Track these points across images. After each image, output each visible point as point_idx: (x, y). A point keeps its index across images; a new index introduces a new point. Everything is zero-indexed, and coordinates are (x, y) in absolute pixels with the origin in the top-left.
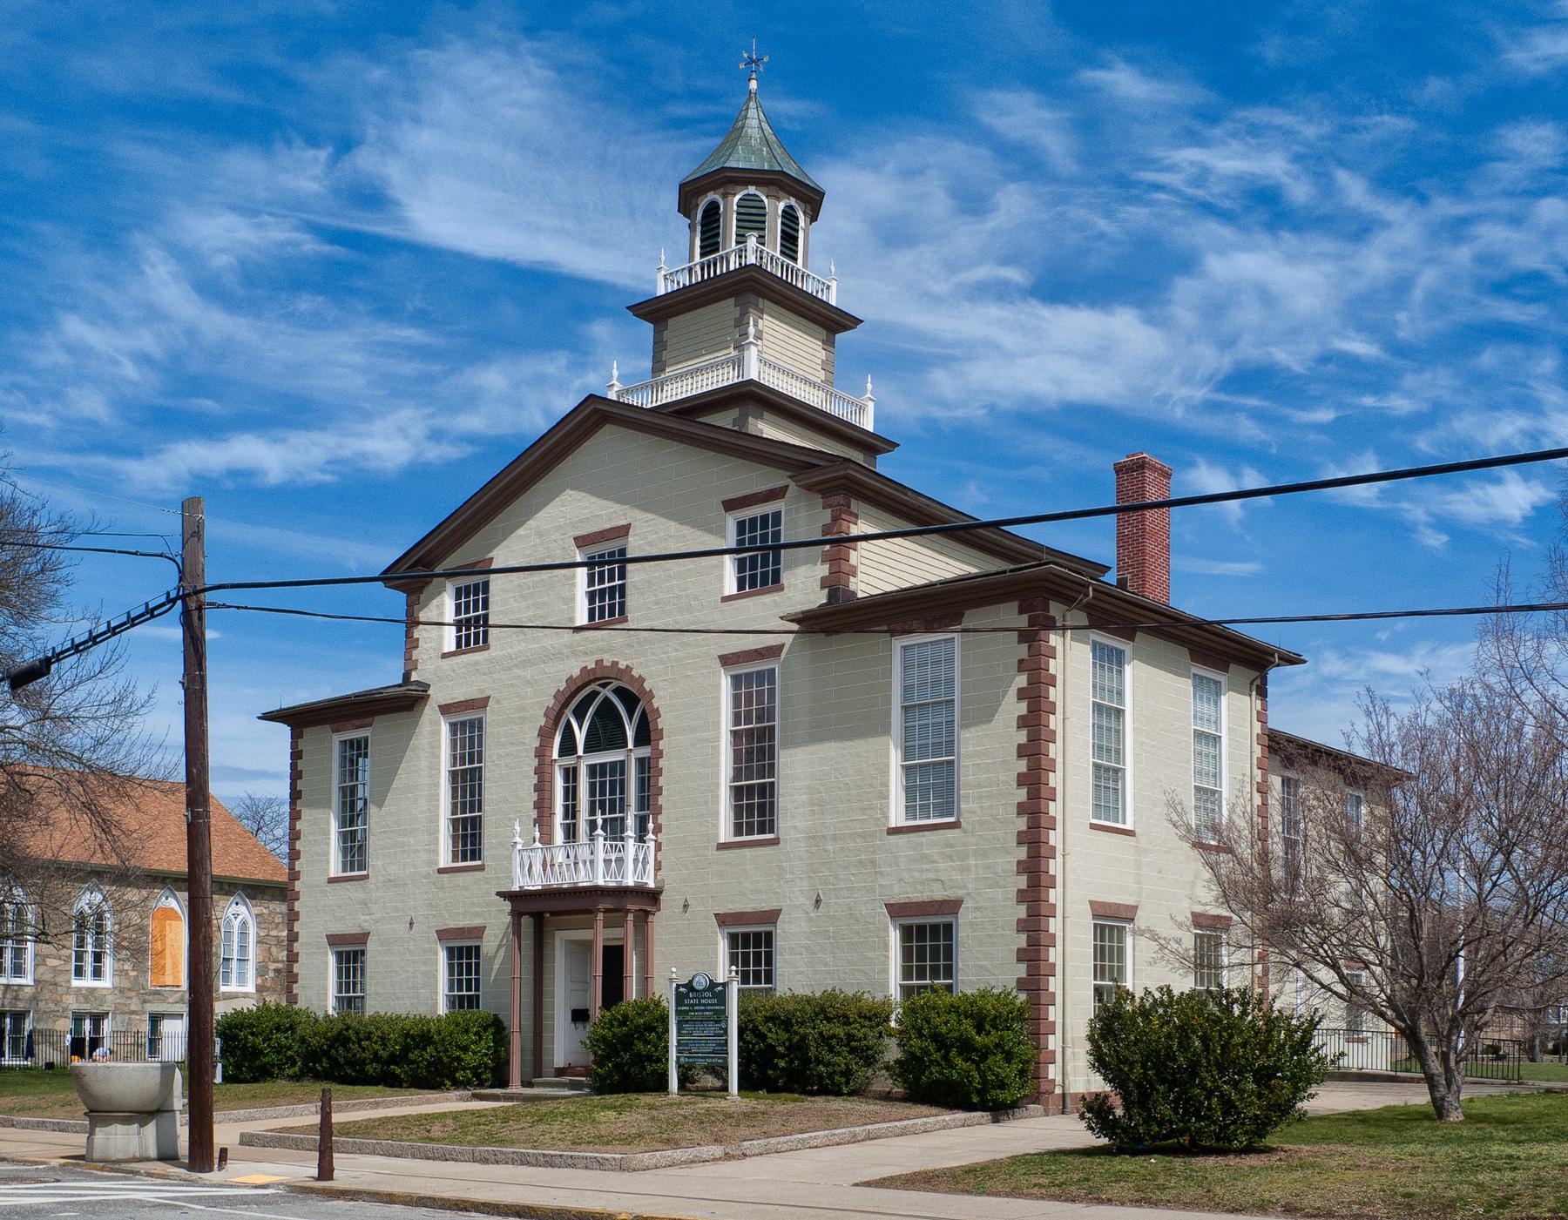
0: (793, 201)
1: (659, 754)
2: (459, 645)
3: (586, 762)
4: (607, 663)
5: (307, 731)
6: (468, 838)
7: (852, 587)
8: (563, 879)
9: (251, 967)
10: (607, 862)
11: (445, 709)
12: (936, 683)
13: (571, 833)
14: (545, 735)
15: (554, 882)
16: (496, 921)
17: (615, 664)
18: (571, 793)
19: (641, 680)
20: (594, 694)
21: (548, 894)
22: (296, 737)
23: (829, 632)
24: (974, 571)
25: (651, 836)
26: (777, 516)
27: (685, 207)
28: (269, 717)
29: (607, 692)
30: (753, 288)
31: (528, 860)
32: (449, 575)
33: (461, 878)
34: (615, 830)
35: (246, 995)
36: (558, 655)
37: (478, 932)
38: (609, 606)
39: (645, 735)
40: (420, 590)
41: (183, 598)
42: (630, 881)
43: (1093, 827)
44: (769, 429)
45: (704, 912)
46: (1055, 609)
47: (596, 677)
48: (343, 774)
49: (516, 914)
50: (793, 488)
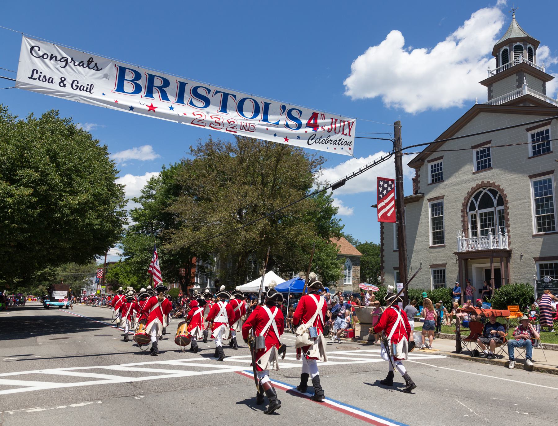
0: (530, 45)
3: (479, 212)
4: (485, 182)
6: (439, 237)
9: (351, 278)
10: (493, 242)
11: (429, 200)
13: (475, 234)
15: (470, 249)
17: (489, 182)
19: (499, 186)
20: (481, 192)
21: (468, 253)
25: (506, 234)
26: (547, 131)
32: (429, 162)
35: (350, 285)
36: (467, 181)
40: (420, 167)
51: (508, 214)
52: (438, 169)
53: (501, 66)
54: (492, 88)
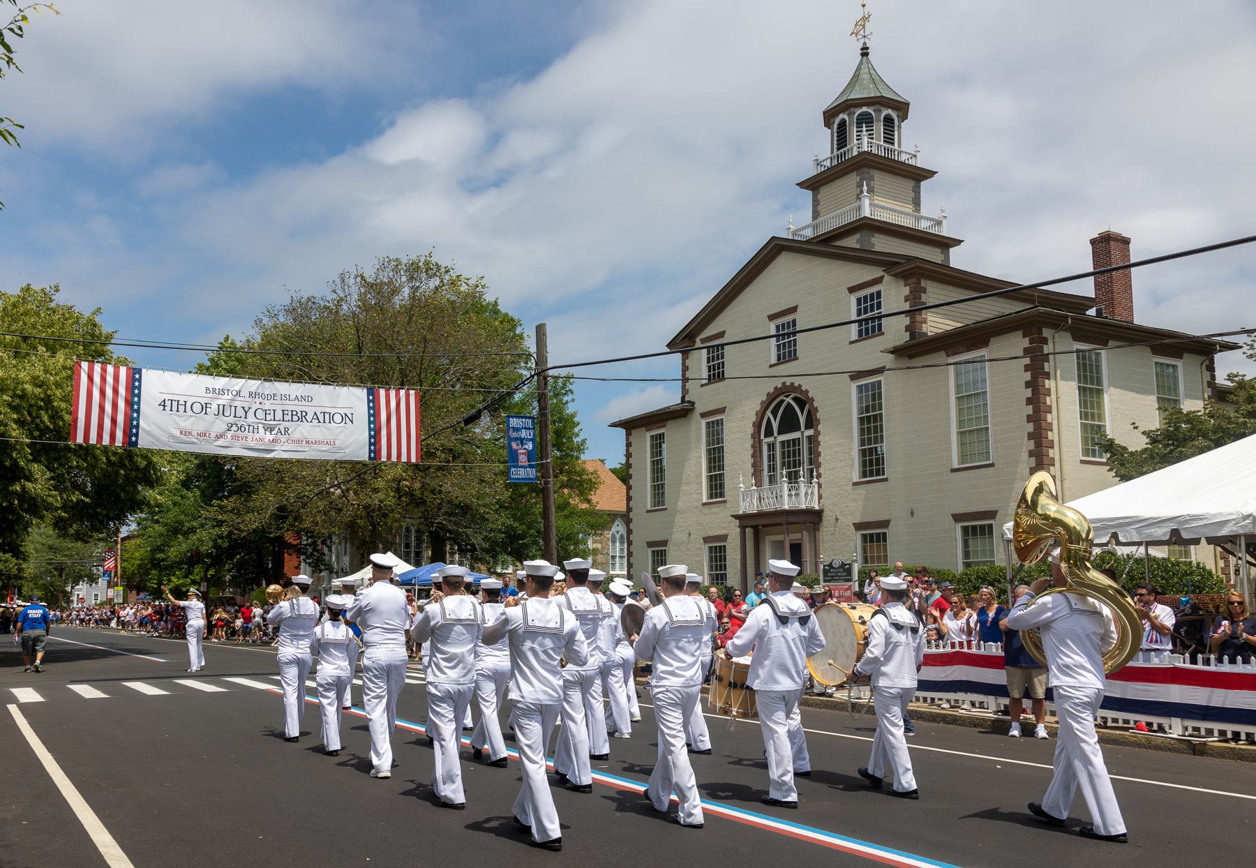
0: (890, 111)
1: (818, 433)
2: (779, 359)
5: (634, 432)
6: (717, 487)
7: (924, 330)
8: (769, 505)
10: (790, 495)
11: (703, 415)
12: (975, 382)
13: (772, 480)
14: (757, 426)
15: (765, 508)
16: (734, 531)
18: (772, 458)
19: (807, 391)
20: (782, 401)
21: (761, 515)
22: (628, 434)
23: (911, 357)
24: (959, 325)
27: (828, 124)
28: (614, 425)
29: (789, 400)
30: (866, 164)
31: (746, 496)
33: (715, 509)
34: (793, 478)
37: (724, 538)
38: (787, 354)
39: (811, 422)
41: (538, 374)
42: (804, 507)
43: (1082, 462)
44: (881, 244)
45: (848, 521)
46: (1046, 333)
47: (784, 390)
48: (652, 453)
49: (743, 528)
50: (887, 278)
51: (819, 443)
52: (872, 306)
53: (835, 152)
54: (819, 197)
